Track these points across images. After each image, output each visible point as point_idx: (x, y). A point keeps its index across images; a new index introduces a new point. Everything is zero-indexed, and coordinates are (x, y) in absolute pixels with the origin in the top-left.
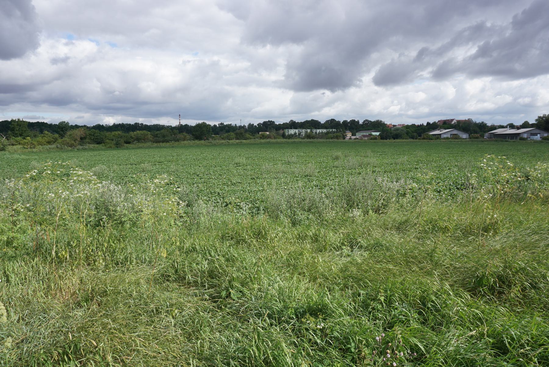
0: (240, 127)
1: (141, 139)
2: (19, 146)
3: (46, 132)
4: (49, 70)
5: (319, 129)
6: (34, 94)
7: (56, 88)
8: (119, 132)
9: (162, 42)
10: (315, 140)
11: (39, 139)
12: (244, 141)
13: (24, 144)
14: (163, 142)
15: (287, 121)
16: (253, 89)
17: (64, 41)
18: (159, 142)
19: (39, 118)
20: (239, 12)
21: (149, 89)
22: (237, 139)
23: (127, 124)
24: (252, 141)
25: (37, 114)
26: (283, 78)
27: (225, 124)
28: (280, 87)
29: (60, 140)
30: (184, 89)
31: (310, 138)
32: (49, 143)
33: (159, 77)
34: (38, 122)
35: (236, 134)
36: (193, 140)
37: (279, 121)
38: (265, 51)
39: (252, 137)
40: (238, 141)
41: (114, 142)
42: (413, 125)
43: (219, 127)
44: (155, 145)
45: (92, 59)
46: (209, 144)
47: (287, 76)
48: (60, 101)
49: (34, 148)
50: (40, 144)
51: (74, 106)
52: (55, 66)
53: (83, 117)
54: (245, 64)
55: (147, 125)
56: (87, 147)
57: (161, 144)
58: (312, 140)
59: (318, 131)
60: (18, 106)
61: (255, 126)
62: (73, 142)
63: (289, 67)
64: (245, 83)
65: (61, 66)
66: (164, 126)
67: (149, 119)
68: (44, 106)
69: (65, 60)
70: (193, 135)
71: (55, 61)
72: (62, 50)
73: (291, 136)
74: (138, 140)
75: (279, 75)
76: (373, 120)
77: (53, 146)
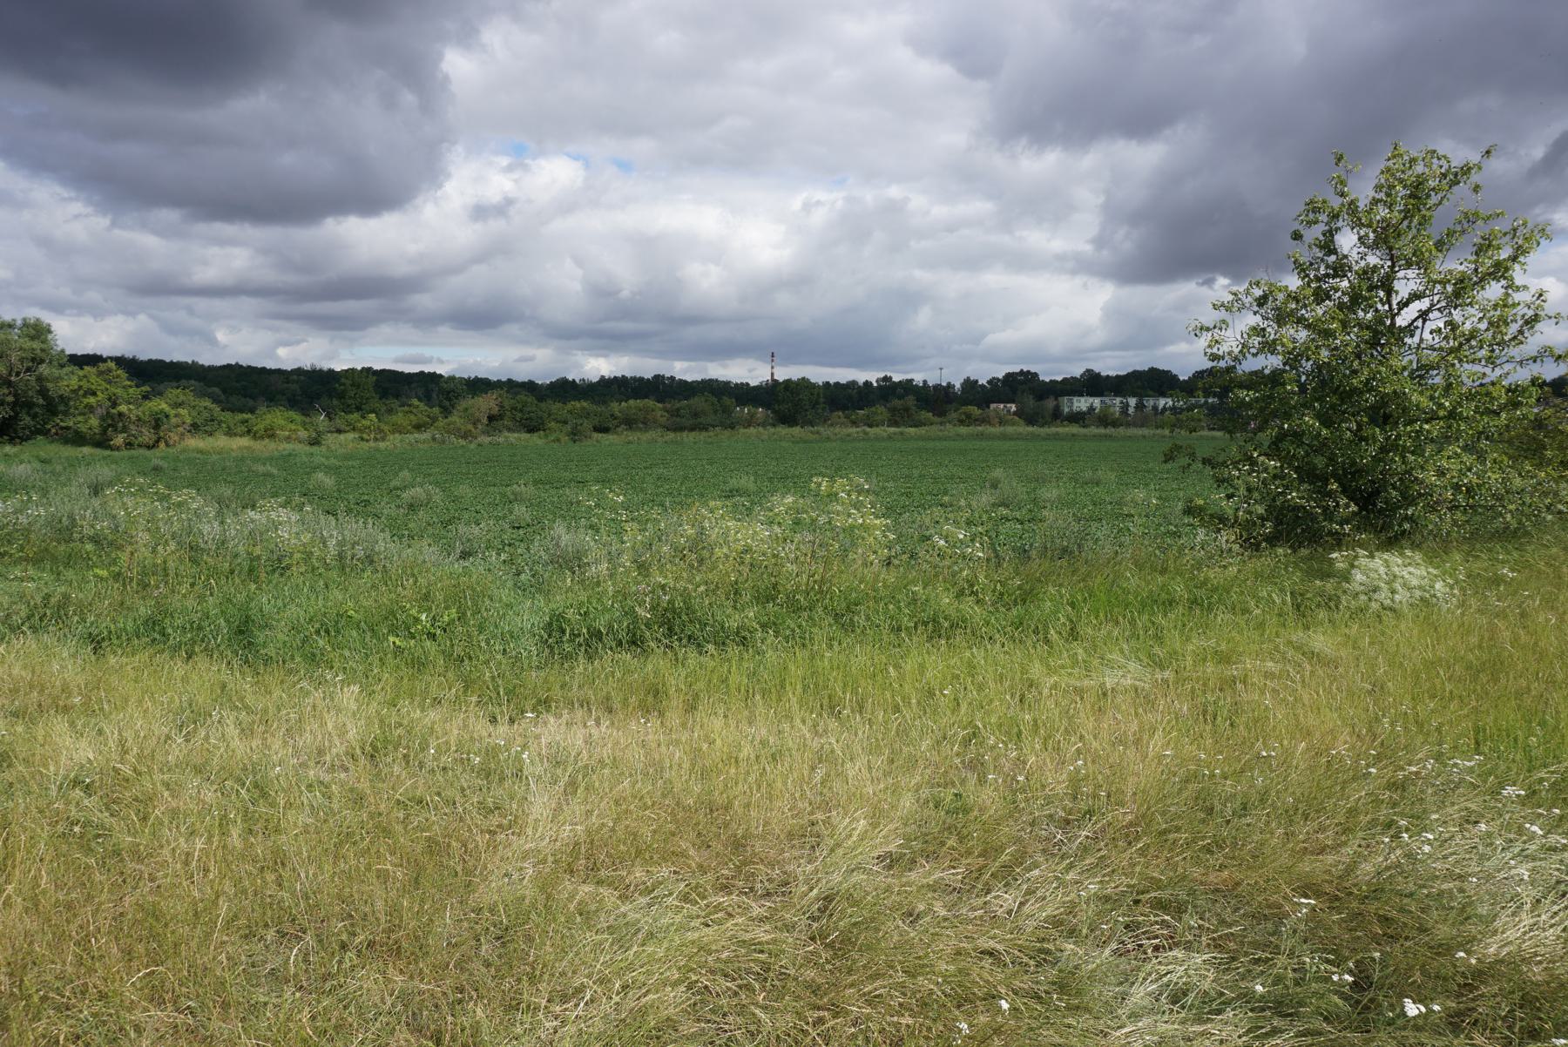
0: (937, 387)
2: (351, 435)
3: (415, 402)
4: (464, 236)
5: (1163, 395)
7: (477, 283)
9: (748, 154)
10: (1121, 430)
11: (399, 418)
12: (912, 430)
14: (692, 429)
15: (1077, 371)
16: (994, 279)
17: (504, 161)
18: (681, 429)
19: (429, 361)
20: (969, 54)
21: (706, 281)
22: (895, 424)
23: (634, 379)
24: (934, 430)
25: (427, 352)
26: (1088, 248)
27: (896, 378)
28: (1074, 272)
29: (441, 423)
30: (799, 281)
32: (418, 427)
33: (734, 245)
35: (893, 410)
37: (1049, 373)
38: (1039, 165)
40: (892, 429)
41: (569, 428)
42: (368, 371)
43: (879, 387)
44: (671, 435)
45: (567, 205)
47: (1100, 242)
48: (480, 318)
49: (383, 439)
50: (398, 429)
51: (514, 329)
52: (478, 226)
53: (531, 359)
54: (980, 207)
56: (501, 440)
57: (685, 434)
58: (1110, 430)
60: (386, 330)
62: (470, 427)
63: (1113, 213)
64: (973, 262)
65: (496, 225)
66: (729, 383)
67: (702, 363)
68: (444, 330)
69: (502, 209)
70: (774, 412)
71: (480, 212)
72: (498, 185)
73: (1077, 418)
74: (630, 423)
75: (1076, 237)
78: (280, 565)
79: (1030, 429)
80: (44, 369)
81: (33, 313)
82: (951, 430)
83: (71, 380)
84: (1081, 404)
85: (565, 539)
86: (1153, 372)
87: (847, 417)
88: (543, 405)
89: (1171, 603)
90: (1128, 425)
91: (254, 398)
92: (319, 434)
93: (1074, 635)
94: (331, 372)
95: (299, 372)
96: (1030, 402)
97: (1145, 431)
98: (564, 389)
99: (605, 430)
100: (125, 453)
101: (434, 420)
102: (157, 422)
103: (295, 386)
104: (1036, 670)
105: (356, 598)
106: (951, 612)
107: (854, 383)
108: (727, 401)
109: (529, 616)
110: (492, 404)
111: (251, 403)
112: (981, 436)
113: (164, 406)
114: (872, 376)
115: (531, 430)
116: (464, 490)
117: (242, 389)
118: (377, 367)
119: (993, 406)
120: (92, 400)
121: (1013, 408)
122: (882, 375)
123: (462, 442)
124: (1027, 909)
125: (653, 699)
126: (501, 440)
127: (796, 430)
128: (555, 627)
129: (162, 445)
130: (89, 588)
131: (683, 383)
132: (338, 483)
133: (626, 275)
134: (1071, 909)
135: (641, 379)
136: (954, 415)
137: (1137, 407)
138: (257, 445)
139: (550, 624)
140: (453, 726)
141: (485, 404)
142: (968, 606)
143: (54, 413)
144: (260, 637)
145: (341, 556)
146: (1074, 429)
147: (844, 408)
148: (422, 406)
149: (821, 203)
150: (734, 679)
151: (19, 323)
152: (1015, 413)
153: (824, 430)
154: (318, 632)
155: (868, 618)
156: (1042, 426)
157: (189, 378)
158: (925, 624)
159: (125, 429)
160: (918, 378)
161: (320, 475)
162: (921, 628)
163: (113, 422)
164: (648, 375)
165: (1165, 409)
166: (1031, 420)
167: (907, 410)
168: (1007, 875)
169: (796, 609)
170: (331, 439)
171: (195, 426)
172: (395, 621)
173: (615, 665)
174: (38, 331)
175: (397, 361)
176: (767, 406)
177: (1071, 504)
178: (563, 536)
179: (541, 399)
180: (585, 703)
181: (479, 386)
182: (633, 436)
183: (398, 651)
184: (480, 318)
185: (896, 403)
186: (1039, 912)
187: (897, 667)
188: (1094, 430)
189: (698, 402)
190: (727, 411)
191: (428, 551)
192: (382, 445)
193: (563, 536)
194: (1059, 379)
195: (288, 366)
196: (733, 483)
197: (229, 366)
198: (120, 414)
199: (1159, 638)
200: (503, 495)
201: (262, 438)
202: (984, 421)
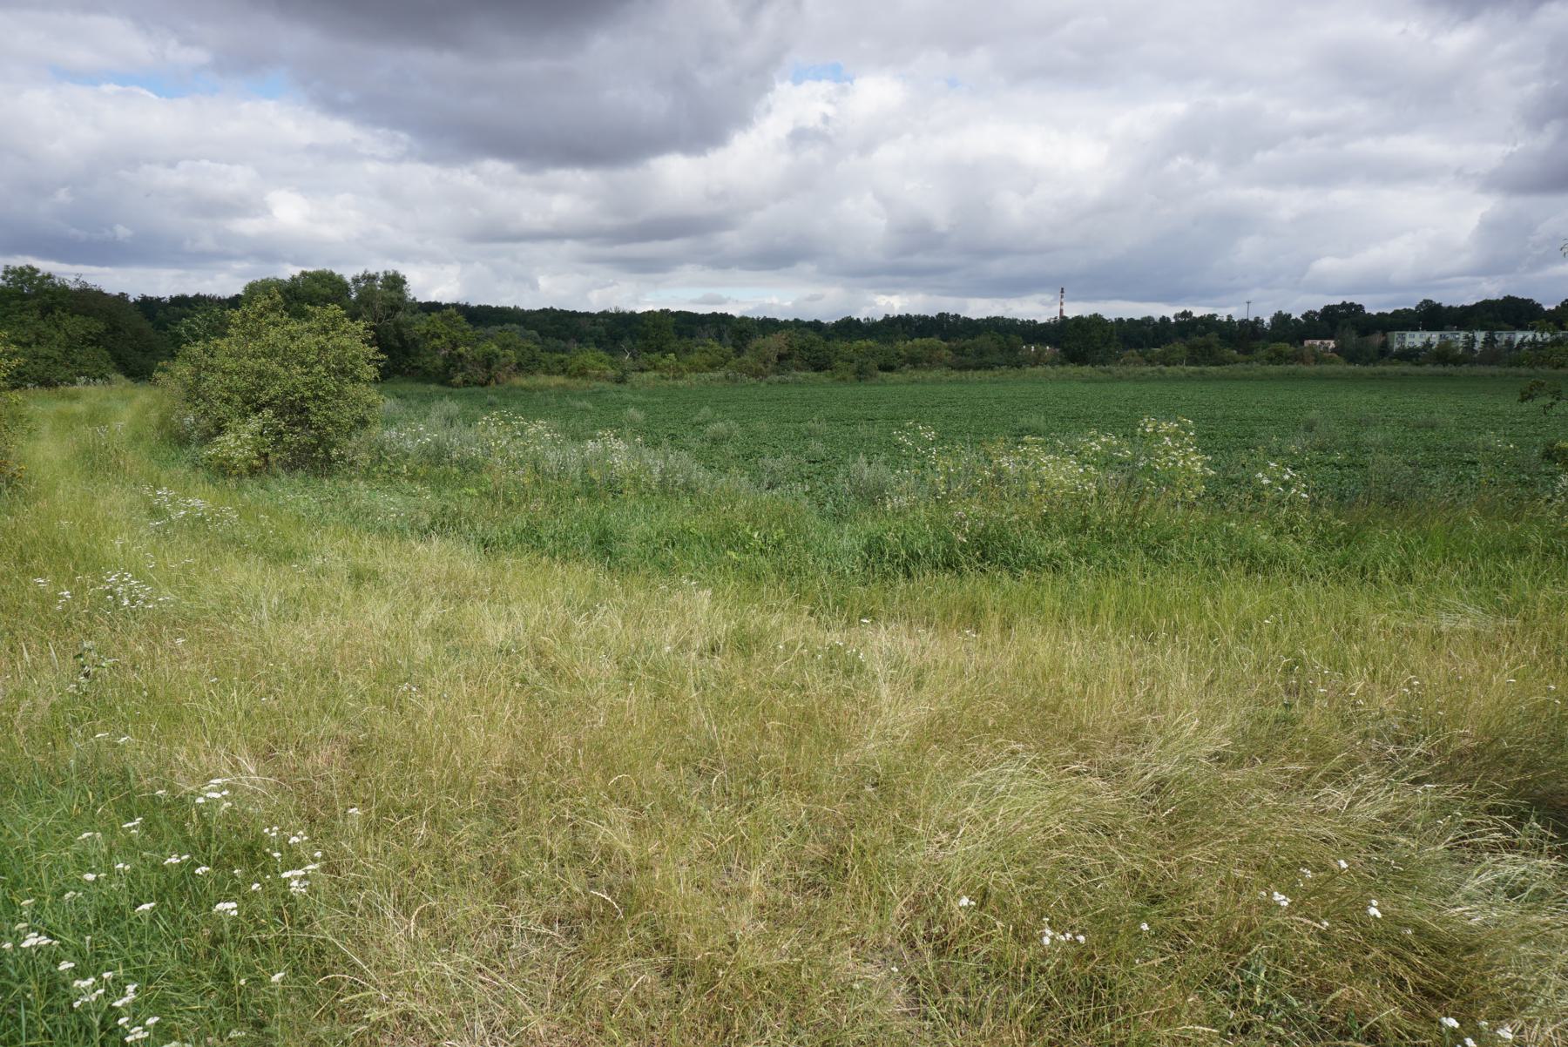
0: (1243, 323)
1: (920, 360)
2: (652, 374)
3: (710, 342)
6: (731, 239)
8: (870, 343)
10: (1465, 368)
11: (695, 358)
13: (661, 370)
14: (977, 368)
15: (1411, 302)
16: (1344, 196)
18: (967, 368)
19: (721, 302)
21: (1015, 210)
22: (1194, 362)
23: (918, 318)
24: (1239, 369)
25: (723, 292)
27: (1198, 312)
29: (734, 362)
31: (1445, 364)
34: (714, 314)
35: (1193, 348)
36: (1062, 364)
39: (1241, 357)
41: (855, 366)
42: (665, 313)
43: (1177, 323)
44: (955, 375)
46: (1102, 376)
49: (681, 377)
50: (695, 369)
51: (808, 268)
55: (970, 320)
56: (790, 378)
57: (970, 373)
59: (1519, 336)
60: (688, 271)
61: (1296, 320)
62: (761, 366)
70: (1064, 350)
71: (799, 137)
73: (1409, 355)
74: (914, 361)
76: (1445, 304)
77: (720, 374)
78: (613, 488)
79: (1351, 367)
80: (400, 316)
81: (391, 266)
82: (1257, 368)
83: (421, 325)
84: (1415, 339)
85: (867, 473)
86: (1509, 300)
87: (1142, 355)
88: (830, 344)
89: (1523, 550)
90: (1473, 362)
91: (565, 339)
92: (624, 372)
93: (1405, 577)
94: (633, 314)
95: (604, 314)
96: (1353, 338)
97: (1495, 370)
98: (849, 328)
99: (889, 369)
100: (463, 390)
101: (728, 359)
102: (488, 362)
103: (601, 329)
104: (1362, 607)
105: (680, 516)
106: (1270, 548)
107: (1149, 320)
108: (1014, 338)
109: (848, 540)
110: (782, 343)
111: (563, 344)
112: (1291, 377)
113: (495, 347)
114: (1168, 311)
115: (818, 369)
116: (762, 426)
117: (559, 330)
118: (674, 309)
119: (1307, 343)
120: (437, 342)
121: (1332, 344)
122: (1181, 311)
123: (753, 380)
124: (1357, 807)
125: (973, 615)
126: (790, 378)
127: (1087, 369)
128: (874, 548)
129: (493, 382)
130: (466, 500)
131: (968, 321)
132: (647, 418)
133: (932, 202)
134: (1405, 808)
135: (926, 318)
136: (1262, 353)
137: (1486, 342)
138: (572, 383)
139: (870, 545)
140: (791, 629)
141: (775, 343)
142: (1288, 544)
143: (407, 354)
144: (617, 548)
145: (662, 483)
146: (1406, 368)
147: (1138, 346)
148: (716, 345)
149: (1158, 111)
150: (1048, 601)
151: (381, 275)
152: (1333, 350)
153: (1116, 369)
154: (666, 544)
155: (1180, 551)
156: (1367, 364)
157: (512, 322)
158: (1243, 560)
159: (463, 369)
160: (1222, 315)
161: (631, 410)
162: (1237, 563)
163: (454, 361)
164: (933, 314)
165: (1522, 343)
166: (1352, 359)
167: (1208, 347)
168: (1336, 778)
169: (1106, 540)
170: (635, 377)
171: (519, 365)
172: (728, 537)
173: (934, 587)
174: (395, 282)
175: (694, 302)
176: (1055, 344)
177: (1402, 449)
178: (865, 470)
179: (828, 338)
180: (906, 616)
181: (768, 326)
182: (918, 375)
183: (737, 565)
184: (775, 258)
185: (1197, 340)
186: (1367, 812)
187: (1213, 597)
188: (1429, 368)
189: (983, 341)
190: (1013, 349)
191: (736, 480)
192: (680, 383)
193: (865, 470)
194: (1389, 311)
195: (595, 309)
196: (1023, 422)
197: (544, 311)
198: (460, 356)
199: (1505, 586)
200: (797, 431)
201: (575, 376)
202: (1298, 358)
